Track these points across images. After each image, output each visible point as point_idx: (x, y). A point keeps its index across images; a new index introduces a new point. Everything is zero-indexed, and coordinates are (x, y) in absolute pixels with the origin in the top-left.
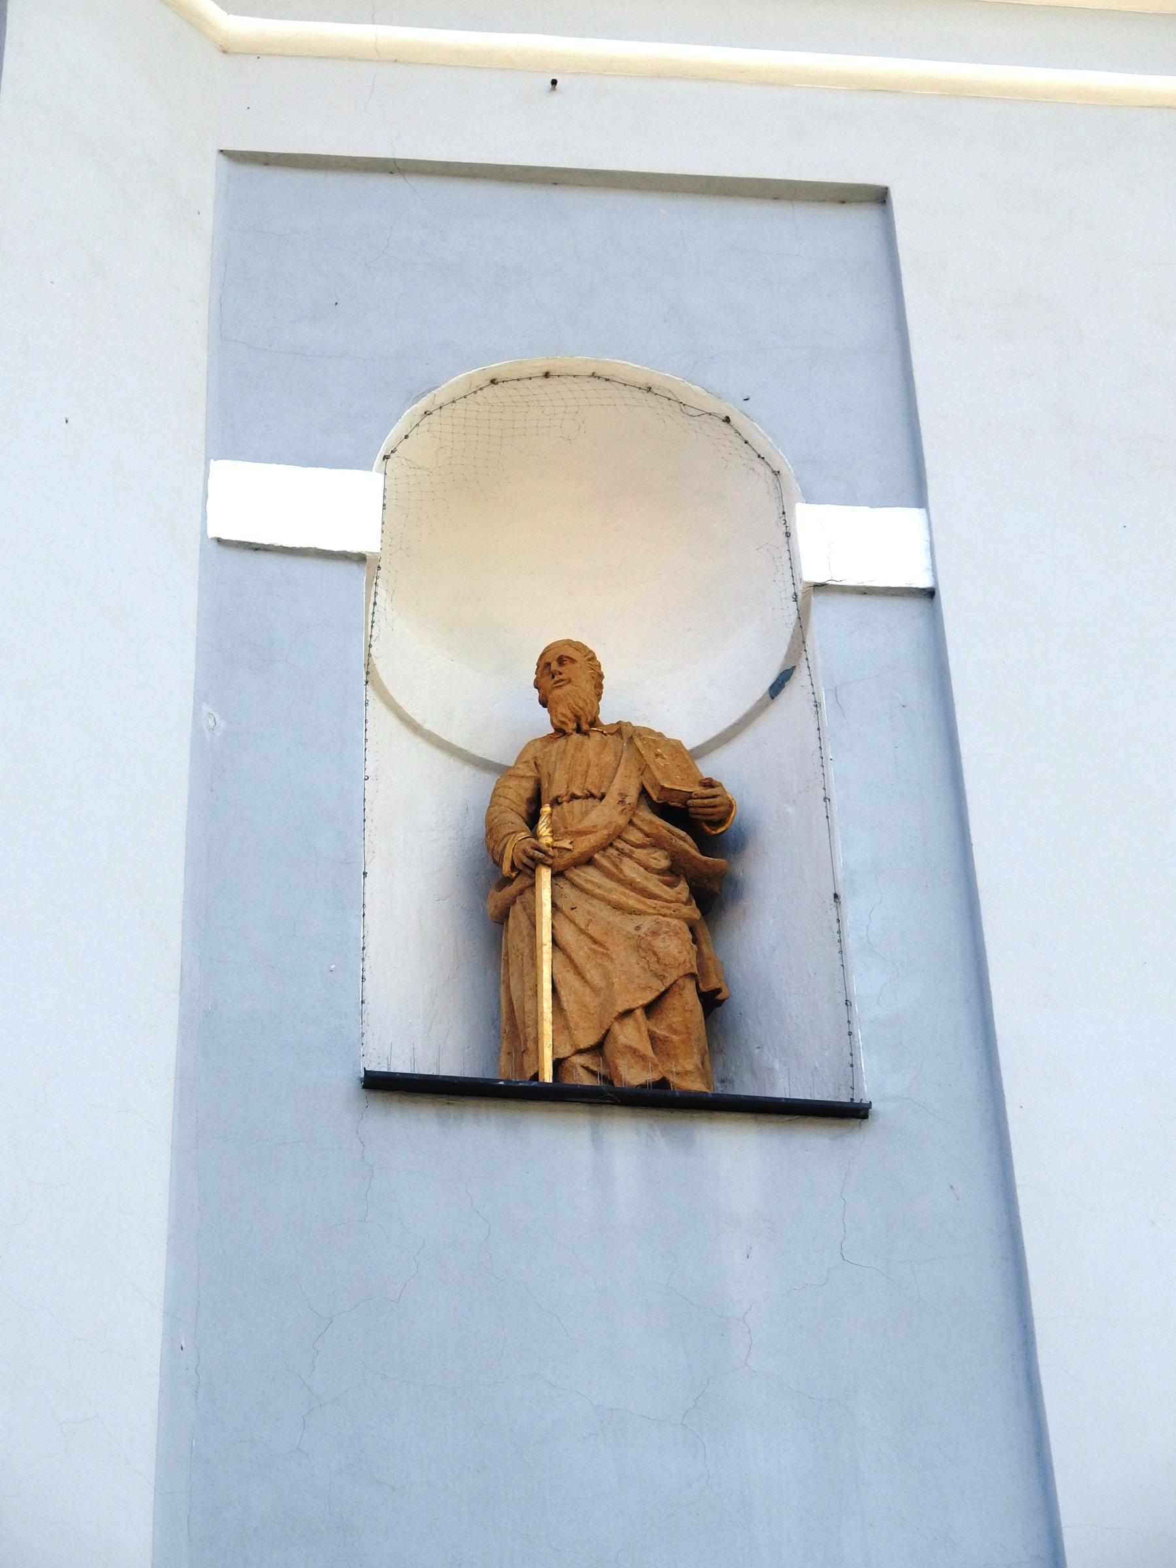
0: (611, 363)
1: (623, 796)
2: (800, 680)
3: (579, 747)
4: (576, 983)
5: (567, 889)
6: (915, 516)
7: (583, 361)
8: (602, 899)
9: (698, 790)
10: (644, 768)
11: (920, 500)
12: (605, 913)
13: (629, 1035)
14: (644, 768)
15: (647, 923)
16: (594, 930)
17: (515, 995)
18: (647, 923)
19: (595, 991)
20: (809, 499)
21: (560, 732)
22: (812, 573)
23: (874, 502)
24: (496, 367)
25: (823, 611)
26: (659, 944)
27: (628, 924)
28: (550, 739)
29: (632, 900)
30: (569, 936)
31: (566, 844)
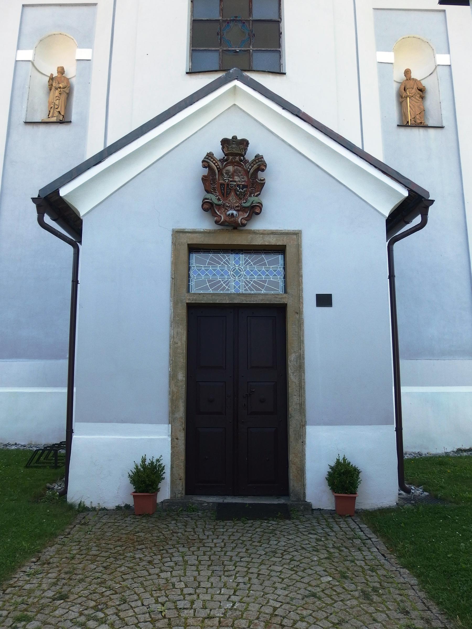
0: (415, 36)
1: (415, 88)
2: (434, 74)
3: (410, 82)
4: (412, 111)
5: (410, 100)
6: (448, 56)
7: (412, 36)
8: (414, 101)
9: (423, 88)
10: (417, 85)
11: (449, 53)
12: (414, 102)
13: (418, 117)
14: (417, 85)
15: (419, 104)
16: (413, 105)
17: (405, 111)
18: (419, 104)
19: (414, 112)
20: (437, 53)
21: (407, 80)
22: (438, 63)
23: (445, 54)
24: (404, 37)
25: (438, 68)
26: (420, 106)
27: (417, 104)
28: (406, 80)
29: (417, 101)
30: (411, 105)
31: (410, 95)
